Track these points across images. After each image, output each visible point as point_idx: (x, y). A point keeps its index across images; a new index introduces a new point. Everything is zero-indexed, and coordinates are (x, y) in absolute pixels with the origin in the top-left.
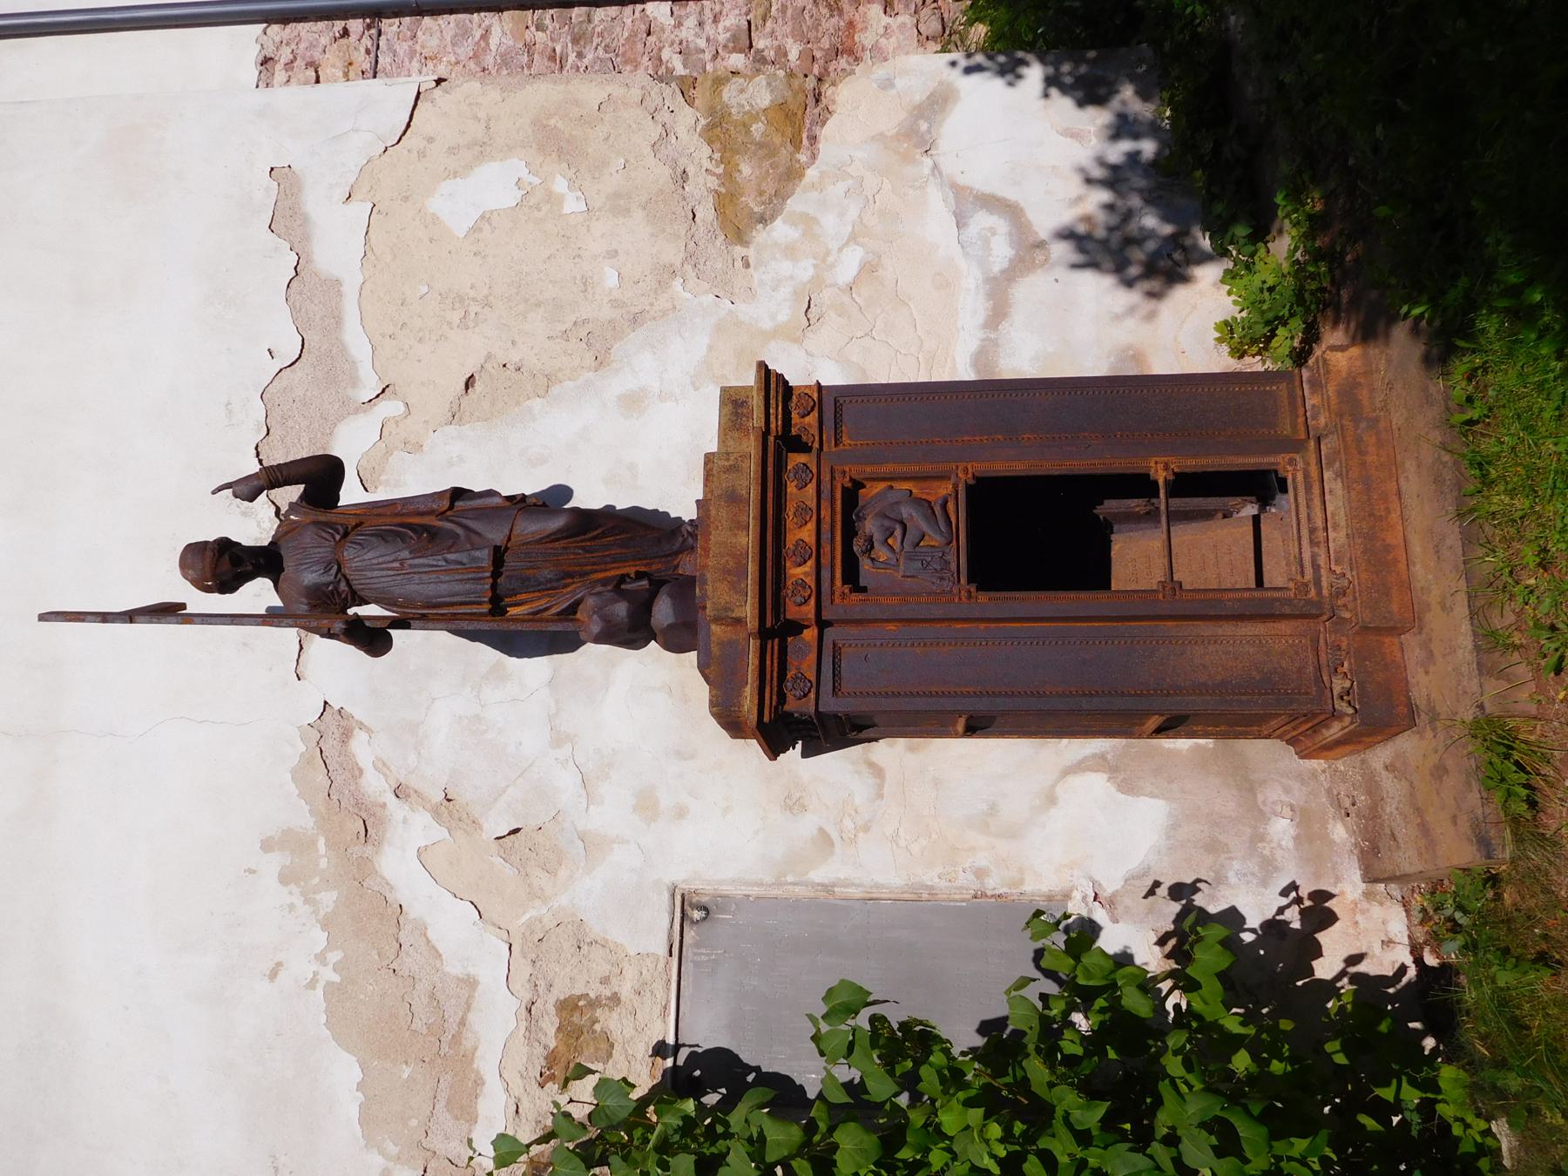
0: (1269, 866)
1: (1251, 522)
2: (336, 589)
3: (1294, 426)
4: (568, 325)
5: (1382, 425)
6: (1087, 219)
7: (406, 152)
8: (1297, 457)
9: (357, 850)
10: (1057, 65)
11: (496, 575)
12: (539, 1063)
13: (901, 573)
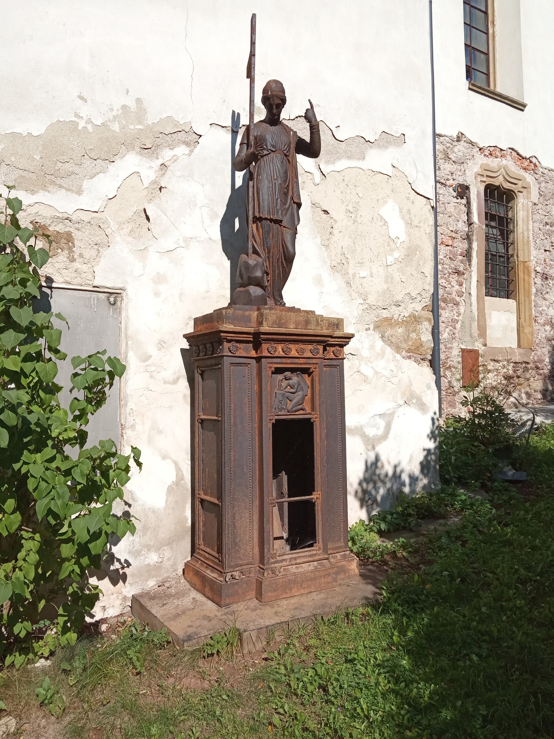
0: (137, 554)
1: (281, 536)
2: (264, 149)
3: (330, 549)
4: (346, 255)
5: (334, 583)
6: (383, 466)
7: (409, 192)
8: (321, 551)
9: (138, 144)
10: (435, 453)
11: (271, 220)
12: (42, 222)
13: (277, 392)
